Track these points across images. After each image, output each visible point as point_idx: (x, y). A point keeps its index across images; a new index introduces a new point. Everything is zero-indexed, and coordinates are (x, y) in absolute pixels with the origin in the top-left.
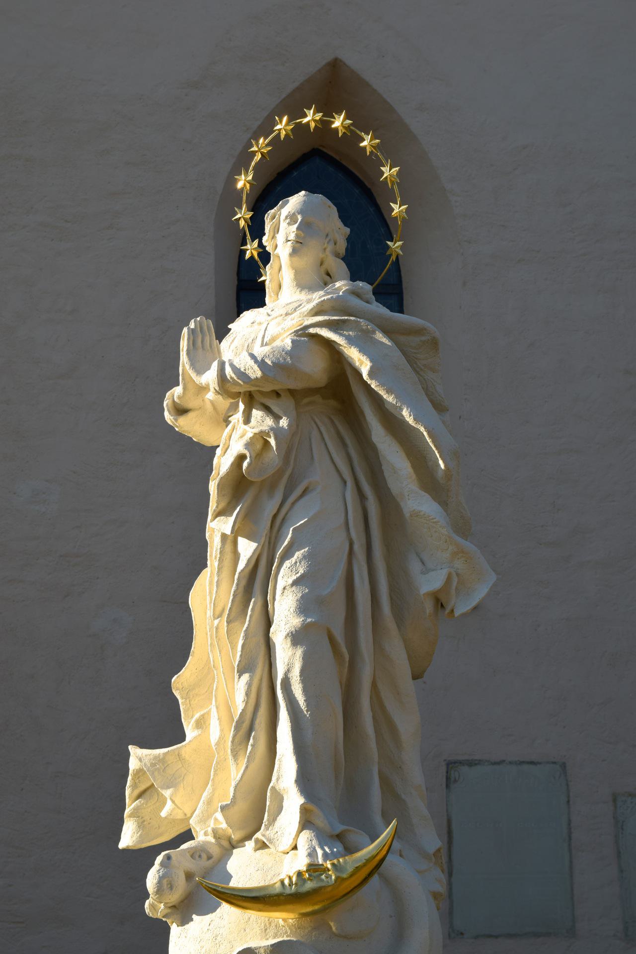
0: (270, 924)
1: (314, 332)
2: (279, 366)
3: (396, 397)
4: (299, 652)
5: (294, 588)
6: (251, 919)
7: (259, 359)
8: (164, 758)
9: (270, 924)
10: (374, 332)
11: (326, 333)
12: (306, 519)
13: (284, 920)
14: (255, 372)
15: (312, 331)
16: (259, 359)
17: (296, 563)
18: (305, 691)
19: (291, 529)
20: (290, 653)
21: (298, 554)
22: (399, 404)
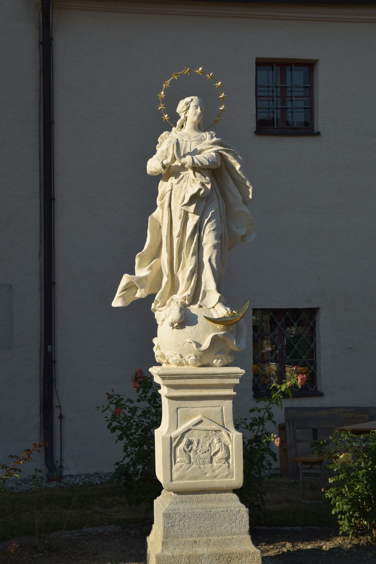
0: (216, 328)
1: (221, 152)
2: (213, 162)
3: (246, 177)
4: (215, 251)
5: (213, 231)
6: (210, 327)
7: (207, 158)
8: (142, 279)
9: (216, 328)
10: (238, 155)
11: (224, 153)
12: (213, 211)
13: (219, 327)
14: (207, 163)
15: (220, 151)
16: (207, 158)
17: (213, 224)
18: (216, 263)
19: (210, 213)
20: (212, 251)
21: (213, 221)
22: (246, 179)
